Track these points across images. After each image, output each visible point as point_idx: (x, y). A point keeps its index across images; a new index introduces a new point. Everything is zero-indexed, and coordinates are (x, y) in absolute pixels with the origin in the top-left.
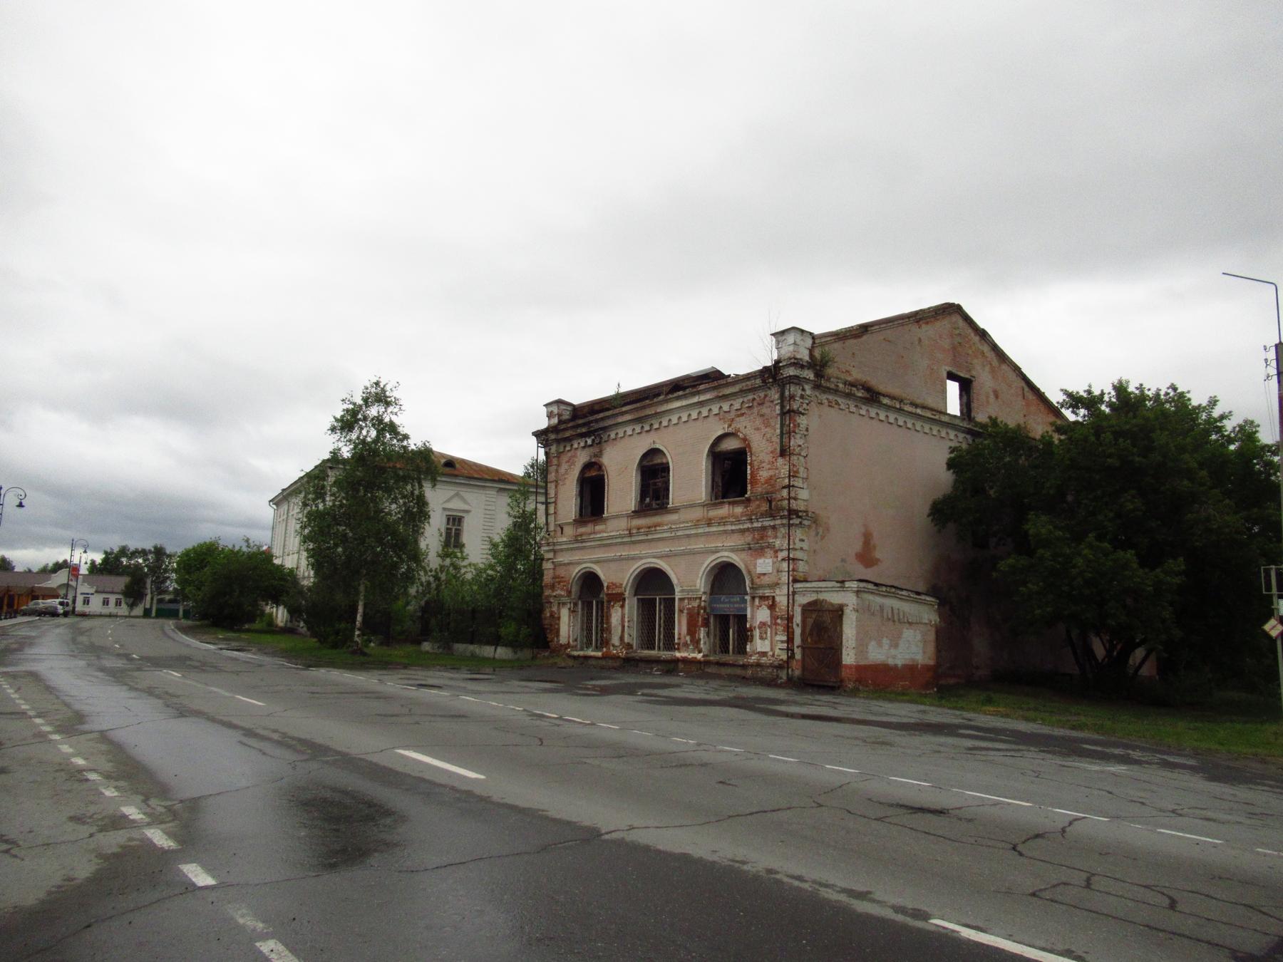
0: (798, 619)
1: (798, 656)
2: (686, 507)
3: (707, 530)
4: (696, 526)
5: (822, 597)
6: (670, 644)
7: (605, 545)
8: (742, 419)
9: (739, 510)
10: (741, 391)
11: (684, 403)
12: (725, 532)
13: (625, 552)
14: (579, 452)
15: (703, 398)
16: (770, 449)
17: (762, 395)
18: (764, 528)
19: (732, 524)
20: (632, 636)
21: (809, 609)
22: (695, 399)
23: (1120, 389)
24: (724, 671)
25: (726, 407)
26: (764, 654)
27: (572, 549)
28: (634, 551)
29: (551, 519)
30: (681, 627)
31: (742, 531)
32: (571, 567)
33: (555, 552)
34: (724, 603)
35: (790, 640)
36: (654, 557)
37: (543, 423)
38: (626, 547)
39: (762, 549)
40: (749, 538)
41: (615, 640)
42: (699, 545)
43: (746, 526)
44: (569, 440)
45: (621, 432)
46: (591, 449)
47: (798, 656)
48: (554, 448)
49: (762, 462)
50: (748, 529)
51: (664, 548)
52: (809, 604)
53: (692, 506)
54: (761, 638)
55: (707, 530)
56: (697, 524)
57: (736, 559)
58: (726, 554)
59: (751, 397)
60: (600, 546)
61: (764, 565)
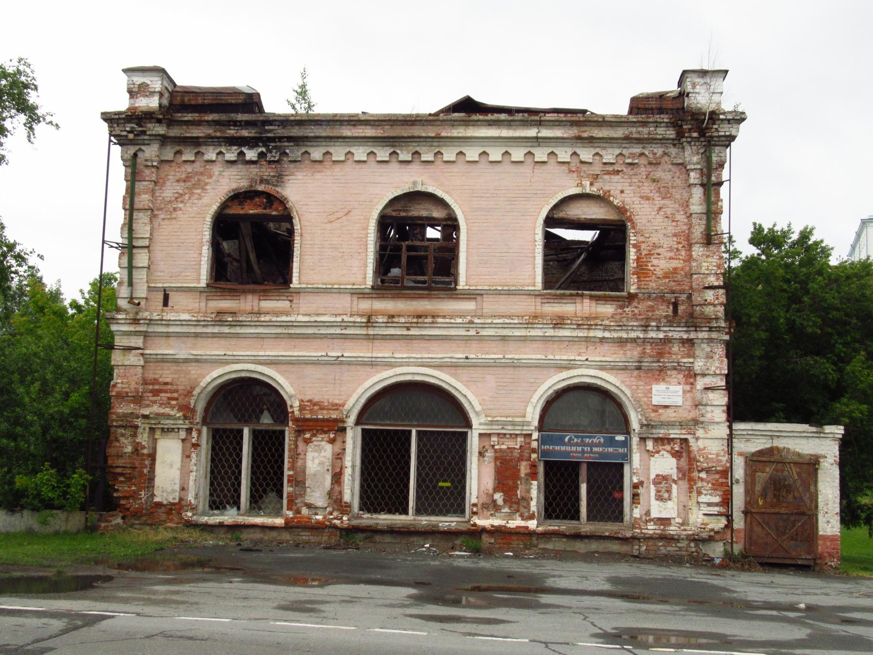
0: (739, 472)
1: (739, 523)
2: (498, 293)
3: (550, 332)
4: (529, 325)
5: (780, 443)
6: (454, 500)
7: (291, 336)
8: (616, 178)
9: (608, 309)
10: (627, 138)
11: (505, 133)
12: (587, 339)
13: (352, 351)
14: (216, 169)
15: (545, 133)
16: (671, 230)
17: (659, 151)
18: (667, 341)
19: (606, 328)
20: (197, 489)
21: (755, 461)
22: (532, 132)
23: (805, 235)
24: (580, 546)
25: (586, 154)
26: (664, 521)
27: (214, 335)
28: (382, 352)
29: (140, 276)
30: (479, 478)
31: (622, 342)
32: (194, 370)
33: (146, 335)
34: (570, 443)
35: (727, 501)
36: (602, 368)
37: (121, 103)
38: (283, 343)
39: (662, 370)
40: (633, 353)
41: (317, 496)
42: (530, 354)
43: (633, 335)
44: (195, 142)
45: (338, 152)
46: (254, 170)
47: (739, 523)
48: (151, 152)
49: (655, 246)
50: (634, 340)
51: (439, 353)
52: (761, 453)
53: (340, 291)
54: (659, 498)
55: (550, 332)
56: (533, 320)
57: (612, 381)
58: (592, 372)
59: (637, 150)
60: (278, 336)
61: (668, 393)
